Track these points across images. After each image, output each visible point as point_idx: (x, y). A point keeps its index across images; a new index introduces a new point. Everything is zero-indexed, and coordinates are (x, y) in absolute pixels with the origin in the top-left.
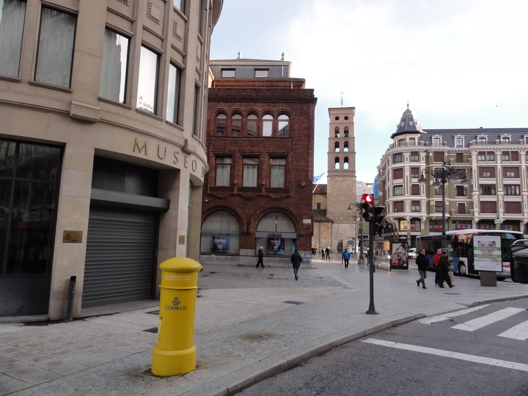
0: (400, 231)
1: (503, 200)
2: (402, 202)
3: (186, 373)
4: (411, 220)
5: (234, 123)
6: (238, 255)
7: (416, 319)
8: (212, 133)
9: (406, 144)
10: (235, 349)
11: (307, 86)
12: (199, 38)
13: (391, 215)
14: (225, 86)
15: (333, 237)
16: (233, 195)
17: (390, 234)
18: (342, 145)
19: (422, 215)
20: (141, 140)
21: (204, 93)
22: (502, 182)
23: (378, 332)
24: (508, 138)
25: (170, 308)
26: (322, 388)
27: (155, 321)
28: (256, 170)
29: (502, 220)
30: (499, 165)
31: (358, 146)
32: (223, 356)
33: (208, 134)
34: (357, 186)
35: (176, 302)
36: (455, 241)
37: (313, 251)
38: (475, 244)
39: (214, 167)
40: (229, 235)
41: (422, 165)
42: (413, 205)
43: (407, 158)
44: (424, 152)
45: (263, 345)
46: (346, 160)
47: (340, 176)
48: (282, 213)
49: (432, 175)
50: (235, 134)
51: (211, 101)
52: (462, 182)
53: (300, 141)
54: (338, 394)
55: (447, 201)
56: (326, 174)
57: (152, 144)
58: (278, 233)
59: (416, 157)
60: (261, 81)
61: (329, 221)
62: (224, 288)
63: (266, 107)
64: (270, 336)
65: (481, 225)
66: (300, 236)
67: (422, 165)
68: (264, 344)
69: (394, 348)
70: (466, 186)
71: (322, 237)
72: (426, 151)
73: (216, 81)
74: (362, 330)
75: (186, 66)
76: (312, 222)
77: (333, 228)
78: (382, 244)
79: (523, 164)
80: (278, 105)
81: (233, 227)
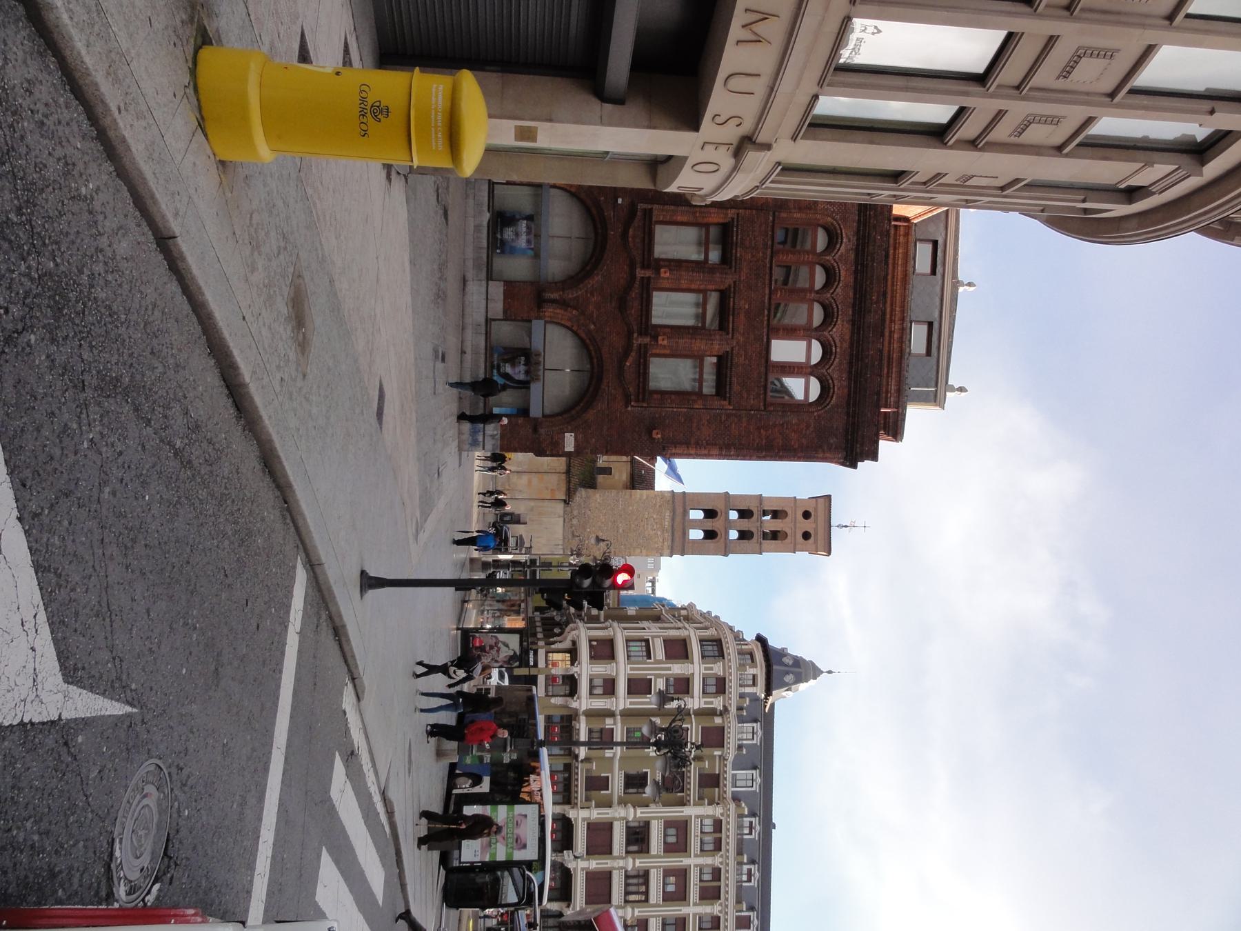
0: (547, 653)
1: (616, 819)
2: (612, 656)
3: (206, 136)
4: (573, 676)
5: (804, 271)
6: (490, 277)
7: (353, 679)
8: (784, 215)
9: (742, 666)
10: (270, 260)
11: (885, 446)
12: (1017, 181)
13: (582, 633)
14: (895, 249)
15: (532, 504)
16: (632, 267)
17: (539, 629)
18: (746, 525)
19: (584, 700)
20: (774, 30)
21: (881, 193)
22: (655, 818)
23: (321, 595)
24: (749, 880)
25: (364, 95)
26: (190, 462)
27: (327, 57)
28: (691, 322)
29: (570, 866)
30: (693, 861)
31: (742, 564)
32: (252, 230)
33: (780, 205)
34: (650, 560)
35: (379, 111)
36: (526, 768)
37: (497, 461)
38: (519, 809)
39: (700, 220)
40: (537, 256)
41: (695, 701)
42: (605, 680)
43: (711, 669)
44: (724, 706)
45: (281, 329)
46: (710, 535)
47: (673, 520)
48: (590, 384)
49: (674, 721)
50: (778, 273)
51: (860, 211)
52: (656, 783)
53: (759, 429)
54: (179, 497)
55: (615, 754)
56: (678, 488)
57: (761, 59)
58: (541, 373)
59: (713, 689)
60: (901, 338)
61: (570, 493)
62: (411, 241)
63: (840, 348)
64: (303, 346)
65: (560, 823)
66: (536, 425)
67: (695, 701)
68: (285, 331)
69: (286, 627)
70: (648, 790)
71: (531, 479)
72: (726, 710)
73: (908, 228)
74: (324, 559)
75: (951, 148)
76: (568, 455)
77: (553, 504)
78: (518, 613)
79: (693, 910)
80: (845, 376)
81: (556, 266)
